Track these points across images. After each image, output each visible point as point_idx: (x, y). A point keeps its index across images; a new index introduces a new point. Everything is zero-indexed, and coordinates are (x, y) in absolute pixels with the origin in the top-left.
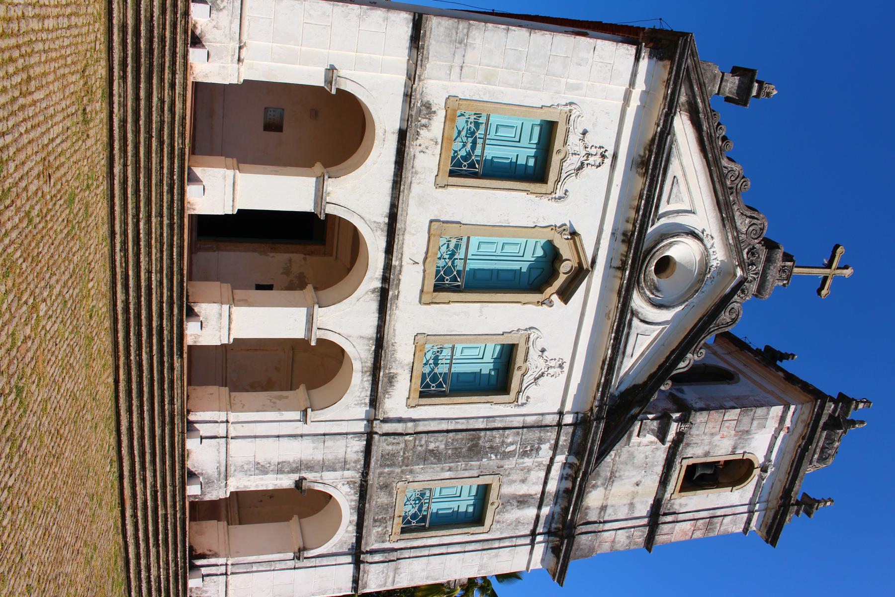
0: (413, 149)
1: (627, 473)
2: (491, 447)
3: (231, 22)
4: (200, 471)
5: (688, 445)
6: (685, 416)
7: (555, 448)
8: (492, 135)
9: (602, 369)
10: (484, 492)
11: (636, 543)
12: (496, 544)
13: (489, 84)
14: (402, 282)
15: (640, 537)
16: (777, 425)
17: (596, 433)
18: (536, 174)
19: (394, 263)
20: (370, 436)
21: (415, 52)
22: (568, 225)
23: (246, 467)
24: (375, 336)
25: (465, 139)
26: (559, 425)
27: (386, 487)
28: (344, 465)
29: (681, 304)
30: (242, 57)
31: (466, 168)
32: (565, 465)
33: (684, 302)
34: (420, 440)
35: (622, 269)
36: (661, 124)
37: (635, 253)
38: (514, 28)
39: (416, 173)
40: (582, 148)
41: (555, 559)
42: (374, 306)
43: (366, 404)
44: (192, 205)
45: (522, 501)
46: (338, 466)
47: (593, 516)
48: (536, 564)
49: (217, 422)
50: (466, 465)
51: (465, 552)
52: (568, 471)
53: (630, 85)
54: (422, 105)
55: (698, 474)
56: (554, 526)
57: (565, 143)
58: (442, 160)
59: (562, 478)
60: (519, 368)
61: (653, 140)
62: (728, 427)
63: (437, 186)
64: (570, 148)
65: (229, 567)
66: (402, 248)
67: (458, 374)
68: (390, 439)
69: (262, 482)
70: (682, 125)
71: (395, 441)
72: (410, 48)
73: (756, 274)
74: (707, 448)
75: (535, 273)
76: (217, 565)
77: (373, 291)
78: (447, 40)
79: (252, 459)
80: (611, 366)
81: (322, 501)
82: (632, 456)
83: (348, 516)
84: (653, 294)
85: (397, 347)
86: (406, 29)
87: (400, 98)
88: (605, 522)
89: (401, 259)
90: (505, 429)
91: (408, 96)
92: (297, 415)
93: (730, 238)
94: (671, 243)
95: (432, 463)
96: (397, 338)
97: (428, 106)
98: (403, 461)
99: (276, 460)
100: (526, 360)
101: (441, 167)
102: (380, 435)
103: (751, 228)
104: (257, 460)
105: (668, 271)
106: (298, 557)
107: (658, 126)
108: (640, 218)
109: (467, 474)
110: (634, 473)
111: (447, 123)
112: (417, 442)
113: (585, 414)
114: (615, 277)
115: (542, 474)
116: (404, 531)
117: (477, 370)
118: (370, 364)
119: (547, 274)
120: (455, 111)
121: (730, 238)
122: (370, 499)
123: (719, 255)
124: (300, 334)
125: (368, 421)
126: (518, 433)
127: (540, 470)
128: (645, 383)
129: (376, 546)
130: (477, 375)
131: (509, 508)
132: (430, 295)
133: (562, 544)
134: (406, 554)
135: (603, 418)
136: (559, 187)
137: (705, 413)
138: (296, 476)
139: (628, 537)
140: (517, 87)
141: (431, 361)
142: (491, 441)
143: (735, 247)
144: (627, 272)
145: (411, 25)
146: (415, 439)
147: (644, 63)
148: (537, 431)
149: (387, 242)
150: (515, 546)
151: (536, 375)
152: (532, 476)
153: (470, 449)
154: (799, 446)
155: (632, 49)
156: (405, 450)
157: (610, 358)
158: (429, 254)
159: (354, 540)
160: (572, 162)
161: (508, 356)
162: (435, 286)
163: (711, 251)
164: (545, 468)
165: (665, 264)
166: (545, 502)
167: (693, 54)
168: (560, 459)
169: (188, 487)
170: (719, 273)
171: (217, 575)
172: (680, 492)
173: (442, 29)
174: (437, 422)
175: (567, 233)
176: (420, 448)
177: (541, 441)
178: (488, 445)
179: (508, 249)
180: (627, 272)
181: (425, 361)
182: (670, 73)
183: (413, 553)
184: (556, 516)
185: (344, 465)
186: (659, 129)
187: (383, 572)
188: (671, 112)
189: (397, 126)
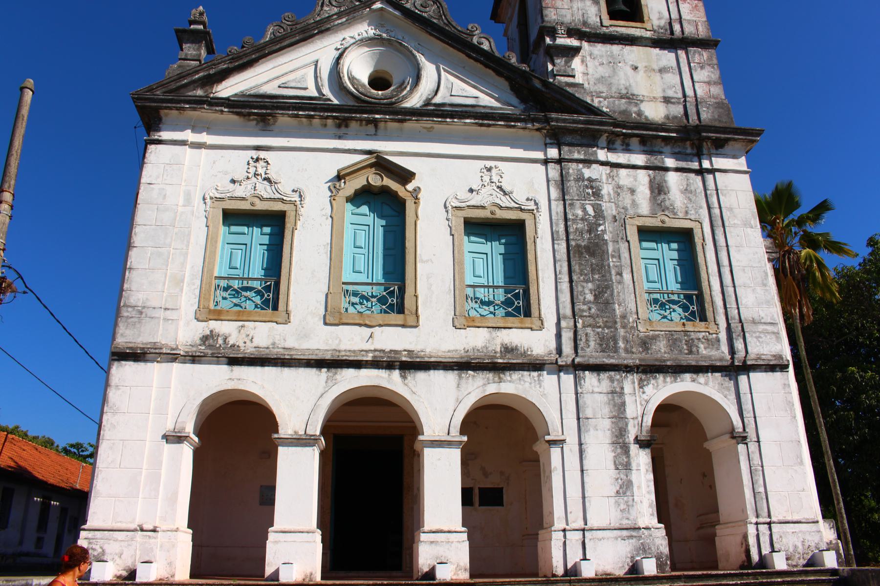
0: (249, 349)
1: (623, 82)
2: (590, 231)
3: (116, 540)
4: (629, 560)
5: (585, 23)
6: (548, 31)
7: (587, 162)
8: (238, 273)
9: (489, 126)
10: (646, 234)
12: (717, 211)
13: (183, 281)
15: (700, 54)
17: (564, 121)
18: (275, 222)
19: (369, 359)
20: (577, 368)
22: (329, 184)
23: (622, 507)
24: (456, 372)
26: (559, 161)
28: (617, 394)
29: (415, 57)
30: (151, 528)
31: (271, 295)
32: (610, 148)
33: (411, 52)
34: (583, 311)
36: (220, 108)
37: (356, 112)
38: (129, 263)
39: (274, 344)
40: (249, 181)
41: (731, 143)
42: (421, 376)
43: (539, 375)
44: (306, 576)
45: (658, 190)
46: (618, 400)
47: (678, 110)
48: (739, 164)
49: (565, 543)
50: (613, 256)
51: (727, 246)
52: (618, 143)
53: (186, 145)
54: (204, 344)
55: (623, 7)
56: (689, 151)
57: (243, 199)
58: (261, 319)
59: (627, 149)
60: (492, 213)
61: (238, 114)
63: (287, 321)
64: (251, 193)
65: (761, 520)
66: (354, 351)
67: (506, 277)
68: (581, 344)
69: (644, 486)
70: (228, 89)
71: (584, 339)
75: (387, 210)
76: (758, 536)
77: (404, 377)
78: (138, 325)
79: (612, 500)
80: (483, 116)
81: (669, 414)
82: (601, 80)
83: (686, 384)
84: (405, 88)
85: (469, 347)
86: (127, 367)
87: (197, 367)
88: (685, 96)
89: (367, 351)
90: (566, 220)
91: (194, 359)
92: (555, 452)
93: (340, 21)
94: (349, 79)
95: (612, 295)
96: (458, 348)
97: (205, 339)
98: (608, 328)
99: (613, 473)
100: (483, 207)
101: (267, 319)
102: (577, 356)
103: (334, 3)
104: (613, 494)
105: (387, 77)
106: (743, 439)
107: (222, 111)
108: (318, 113)
109: (625, 255)
110: (621, 74)
111: (222, 318)
112: (585, 314)
113: (546, 136)
114: (386, 128)
115: (623, 172)
116: (703, 318)
117: (500, 258)
118: (490, 375)
119: (385, 198)
120: (210, 311)
121: (340, 21)
122: (660, 361)
123: (364, 29)
124: (455, 454)
125: (560, 371)
126: (571, 205)
128: (507, 79)
129: (725, 348)
130: (506, 257)
131: (667, 203)
133: (709, 138)
134: (733, 313)
135: (545, 116)
136: (288, 199)
137: (545, 12)
138: (634, 449)
139: (702, 68)
140: (187, 254)
141: (492, 309)
142: (581, 233)
144: (377, 116)
145: (123, 362)
146: (581, 316)
147: (165, 135)
149: (348, 367)
150: (717, 190)
151: (500, 194)
152: (625, 183)
153: (592, 254)
155: (152, 148)
156: (594, 326)
157: (475, 119)
158: (361, 322)
159: (718, 375)
160: (264, 190)
161: (479, 227)
162: (701, 320)
163: (358, 38)
164: (615, 170)
165: (378, 81)
166: (659, 164)
167: (151, 90)
168: (602, 155)
169: (646, 573)
170: (382, 26)
171: (771, 535)
172: (643, 22)
173: (128, 332)
174: (560, 295)
175: (338, 184)
176: (593, 310)
177: (580, 178)
178: (586, 236)
179: (361, 242)
180: (377, 116)
181: (492, 316)
183: (732, 304)
185: (617, 394)
186: (226, 110)
187: (757, 338)
188: (207, 101)
189: (225, 368)
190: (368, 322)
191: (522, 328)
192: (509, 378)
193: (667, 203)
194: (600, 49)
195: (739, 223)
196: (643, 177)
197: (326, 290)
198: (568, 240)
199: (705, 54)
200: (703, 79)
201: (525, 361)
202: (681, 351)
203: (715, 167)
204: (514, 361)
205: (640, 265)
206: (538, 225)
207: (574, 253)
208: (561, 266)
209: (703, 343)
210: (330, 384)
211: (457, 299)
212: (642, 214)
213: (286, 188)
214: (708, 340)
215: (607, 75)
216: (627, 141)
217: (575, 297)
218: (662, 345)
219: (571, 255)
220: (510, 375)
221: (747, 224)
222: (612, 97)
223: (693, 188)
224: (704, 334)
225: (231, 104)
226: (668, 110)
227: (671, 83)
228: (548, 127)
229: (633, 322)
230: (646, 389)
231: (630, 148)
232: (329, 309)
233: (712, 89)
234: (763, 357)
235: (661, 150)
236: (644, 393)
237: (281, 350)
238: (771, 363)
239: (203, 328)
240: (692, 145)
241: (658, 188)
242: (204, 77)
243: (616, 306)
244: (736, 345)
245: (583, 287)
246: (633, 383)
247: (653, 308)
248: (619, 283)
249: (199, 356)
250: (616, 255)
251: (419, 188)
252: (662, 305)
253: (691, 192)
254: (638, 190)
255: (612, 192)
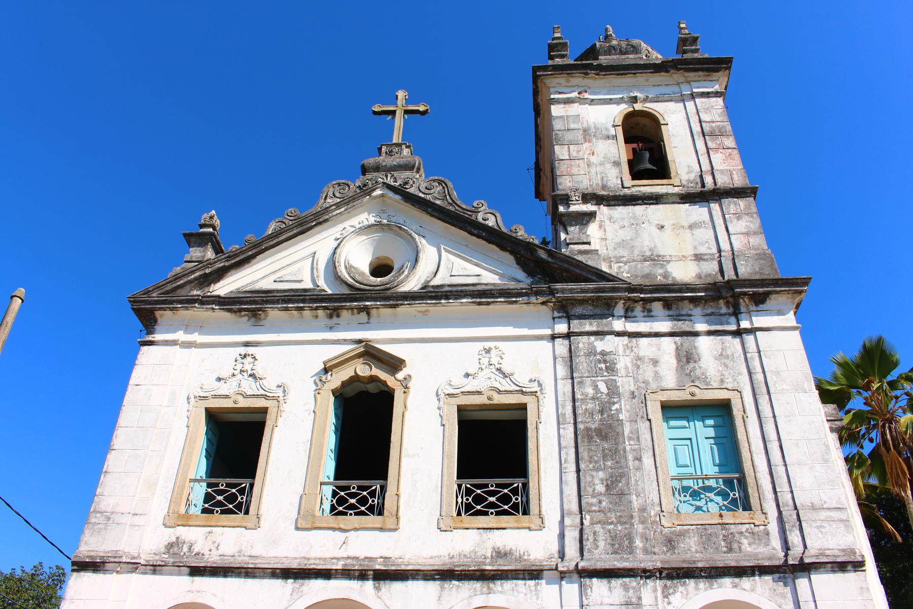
0: (212, 558)
2: (601, 412)
5: (604, 187)
6: (561, 199)
9: (488, 304)
10: (671, 410)
11: (748, 207)
14: (369, 555)
15: (735, 204)
16: (576, 105)
17: (571, 291)
19: (339, 567)
21: (108, 566)
24: (438, 582)
25: (703, 501)
27: (670, 542)
32: (628, 315)
33: (412, 237)
34: (592, 505)
35: (367, 310)
37: (345, 300)
38: (105, 467)
40: (234, 379)
41: (773, 296)
42: (397, 587)
45: (686, 358)
50: (630, 439)
51: (774, 417)
53: (176, 344)
54: (168, 552)
56: (724, 310)
57: (227, 397)
58: (230, 524)
59: (649, 315)
60: (489, 399)
61: (229, 310)
62: (578, 152)
68: (588, 545)
70: (223, 288)
71: (591, 538)
72: (105, 571)
73: (387, 176)
74: (608, 166)
77: (378, 589)
78: (103, 532)
80: (482, 294)
82: (622, 244)
87: (157, 578)
88: (720, 251)
89: (338, 559)
90: (574, 400)
91: (155, 568)
93: (338, 211)
94: (346, 267)
95: (628, 484)
96: (441, 553)
97: (170, 546)
98: (622, 523)
101: (236, 524)
105: (384, 262)
107: (213, 309)
109: (645, 436)
111: (190, 523)
112: (594, 508)
114: (379, 316)
115: (644, 341)
116: (747, 507)
118: (478, 585)
121: (338, 211)
123: (366, 218)
125: (562, 578)
126: (580, 383)
127: (637, 346)
128: (512, 252)
129: (776, 542)
131: (698, 372)
132: (387, 519)
133: (745, 294)
134: (785, 497)
135: (549, 287)
136: (271, 395)
139: (739, 218)
143: (348, 202)
148: (576, 360)
149: (316, 578)
150: (759, 352)
151: (499, 377)
152: (646, 357)
154: (598, 74)
155: (145, 349)
157: (473, 298)
158: (335, 526)
159: (768, 578)
162: (744, 509)
163: (358, 226)
164: (634, 340)
165: (381, 269)
167: (147, 292)
168: (618, 325)
174: (564, 487)
176: (604, 504)
177: (591, 352)
178: (598, 417)
182: (164, 309)
184: (709, 311)
187: (817, 527)
189: (187, 579)
190: (342, 526)
191: (518, 528)
192: (499, 588)
193: (698, 372)
194: (621, 212)
195: (788, 388)
196: (668, 344)
197: (301, 491)
198: (575, 423)
199: (742, 203)
200: (738, 236)
201: (518, 567)
202: (717, 548)
203: (756, 325)
204: (506, 568)
205: (666, 449)
206: (541, 408)
207: (583, 437)
208: (567, 454)
209: (746, 538)
210: (295, 596)
211: (444, 497)
212: (667, 387)
213: (270, 384)
214: (753, 533)
215: (629, 238)
216: (648, 307)
217: (582, 488)
218: (692, 543)
219: (579, 440)
220: (502, 585)
221: (798, 388)
222: (634, 261)
223: (729, 353)
224: (747, 526)
225: (228, 303)
226: (700, 268)
227: (704, 240)
228: (554, 300)
229: (655, 516)
230: (672, 598)
231: (653, 314)
232: (302, 512)
233: (751, 240)
234: (828, 552)
235: (690, 312)
236: (669, 603)
237: (247, 559)
238: (839, 560)
239: (169, 535)
240: (727, 304)
241: (687, 356)
242: (200, 276)
243: (634, 497)
244: (790, 538)
245: (593, 477)
246: (655, 590)
247: (683, 499)
248: (638, 469)
249: (159, 566)
250: (635, 436)
251: (410, 376)
252: (695, 494)
253: (727, 357)
254: (662, 360)
255: (630, 365)
